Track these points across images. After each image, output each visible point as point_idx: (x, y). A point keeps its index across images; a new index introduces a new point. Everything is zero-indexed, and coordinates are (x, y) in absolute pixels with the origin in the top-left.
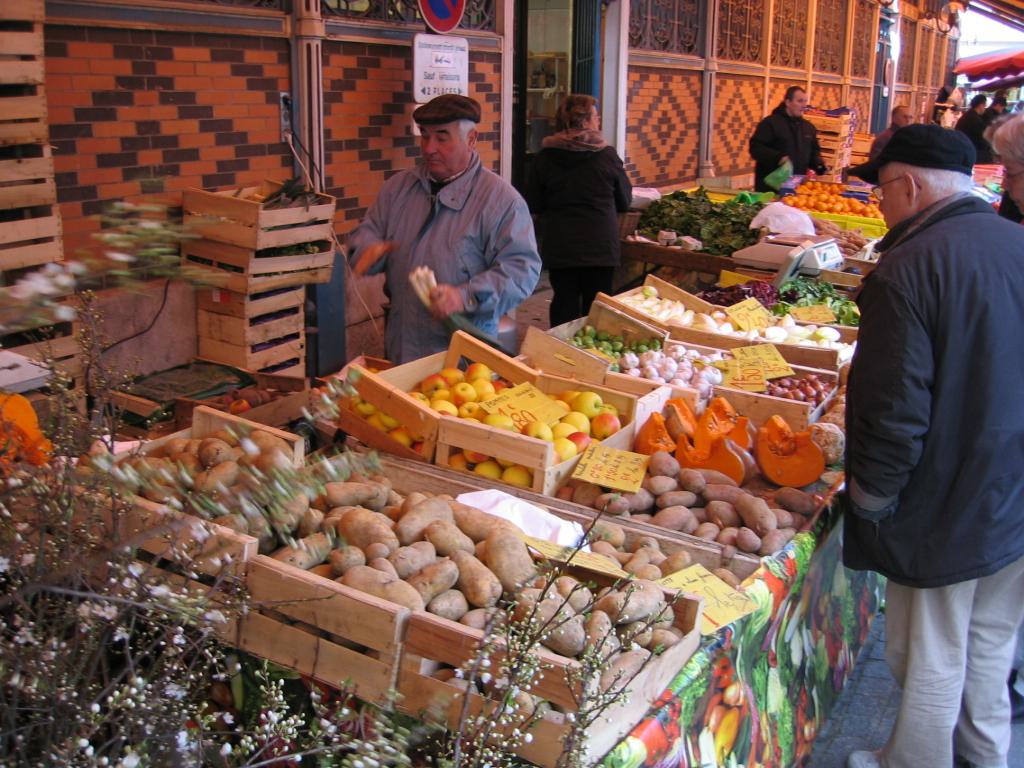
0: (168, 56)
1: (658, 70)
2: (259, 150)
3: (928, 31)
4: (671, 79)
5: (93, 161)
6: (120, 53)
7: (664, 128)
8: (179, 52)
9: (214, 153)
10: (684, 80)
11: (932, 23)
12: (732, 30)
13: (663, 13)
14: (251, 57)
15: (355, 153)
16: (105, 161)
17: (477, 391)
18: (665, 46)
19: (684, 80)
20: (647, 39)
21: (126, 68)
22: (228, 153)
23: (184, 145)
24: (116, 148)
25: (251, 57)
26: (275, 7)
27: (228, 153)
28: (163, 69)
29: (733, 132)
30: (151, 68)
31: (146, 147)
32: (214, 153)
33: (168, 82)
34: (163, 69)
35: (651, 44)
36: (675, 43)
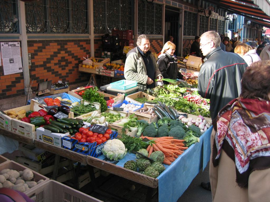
0: (66, 44)
1: (155, 39)
2: (41, 66)
3: (253, 29)
4: (190, 41)
5: (53, 64)
6: (58, 45)
7: (63, 63)
8: (68, 43)
9: (50, 65)
10: (156, 41)
11: (203, 14)
12: (192, 30)
13: (158, 26)
14: (81, 43)
15: (43, 68)
16: (71, 63)
17: (3, 186)
18: (189, 35)
19: (156, 41)
20: (187, 34)
21: (59, 47)
22: (48, 65)
23: (69, 61)
24: (69, 65)
25: (81, 43)
26: (17, 33)
27: (48, 65)
28: (66, 47)
29: (60, 61)
30: (64, 47)
31: (62, 62)
32: (50, 65)
33: (66, 49)
34: (66, 47)
35: (155, 33)
36: (191, 34)
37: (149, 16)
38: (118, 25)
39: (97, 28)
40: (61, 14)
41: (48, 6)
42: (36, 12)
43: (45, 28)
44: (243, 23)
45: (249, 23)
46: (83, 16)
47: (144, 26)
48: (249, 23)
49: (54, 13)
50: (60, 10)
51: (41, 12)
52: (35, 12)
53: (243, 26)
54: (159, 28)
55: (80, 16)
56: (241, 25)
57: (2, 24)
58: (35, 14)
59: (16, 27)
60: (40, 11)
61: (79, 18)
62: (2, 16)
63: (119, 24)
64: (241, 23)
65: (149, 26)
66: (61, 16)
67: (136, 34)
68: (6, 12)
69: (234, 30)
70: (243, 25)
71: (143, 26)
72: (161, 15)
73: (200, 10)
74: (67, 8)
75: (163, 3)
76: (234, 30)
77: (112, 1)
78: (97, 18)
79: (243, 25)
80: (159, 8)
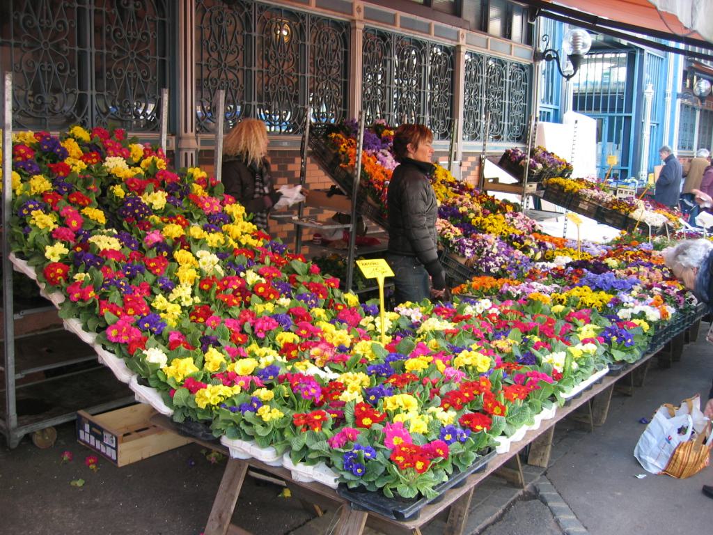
13: (517, 121)
37: (514, 98)
38: (421, 116)
39: (273, 117)
40: (284, 88)
41: (257, 69)
42: (225, 83)
43: (79, 115)
44: (679, 90)
45: (703, 91)
46: (291, 89)
47: (503, 123)
48: (703, 91)
49: (112, 70)
50: (227, 71)
51: (291, 89)
52: (223, 82)
53: (679, 101)
54: (444, 119)
55: (46, 68)
56: (669, 99)
57: (128, 110)
58: (129, 79)
59: (83, 115)
60: (235, 81)
61: (280, 92)
62: (44, 84)
63: (390, 112)
64: (669, 91)
65: (436, 115)
66: (135, 80)
67: (186, 131)
68: (55, 74)
69: (633, 115)
70: (678, 96)
71: (500, 122)
72: (450, 80)
73: (542, 51)
74: (77, 49)
75: (352, 17)
76: (633, 115)
77: (128, 4)
78: (368, 99)
79: (678, 96)
80: (521, 74)
